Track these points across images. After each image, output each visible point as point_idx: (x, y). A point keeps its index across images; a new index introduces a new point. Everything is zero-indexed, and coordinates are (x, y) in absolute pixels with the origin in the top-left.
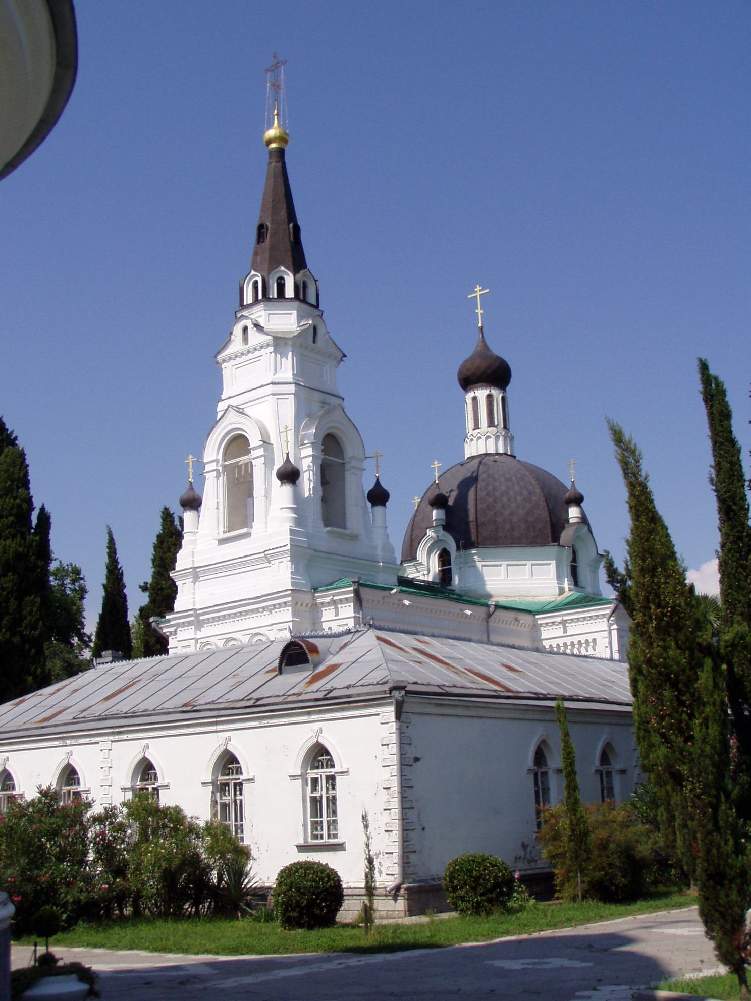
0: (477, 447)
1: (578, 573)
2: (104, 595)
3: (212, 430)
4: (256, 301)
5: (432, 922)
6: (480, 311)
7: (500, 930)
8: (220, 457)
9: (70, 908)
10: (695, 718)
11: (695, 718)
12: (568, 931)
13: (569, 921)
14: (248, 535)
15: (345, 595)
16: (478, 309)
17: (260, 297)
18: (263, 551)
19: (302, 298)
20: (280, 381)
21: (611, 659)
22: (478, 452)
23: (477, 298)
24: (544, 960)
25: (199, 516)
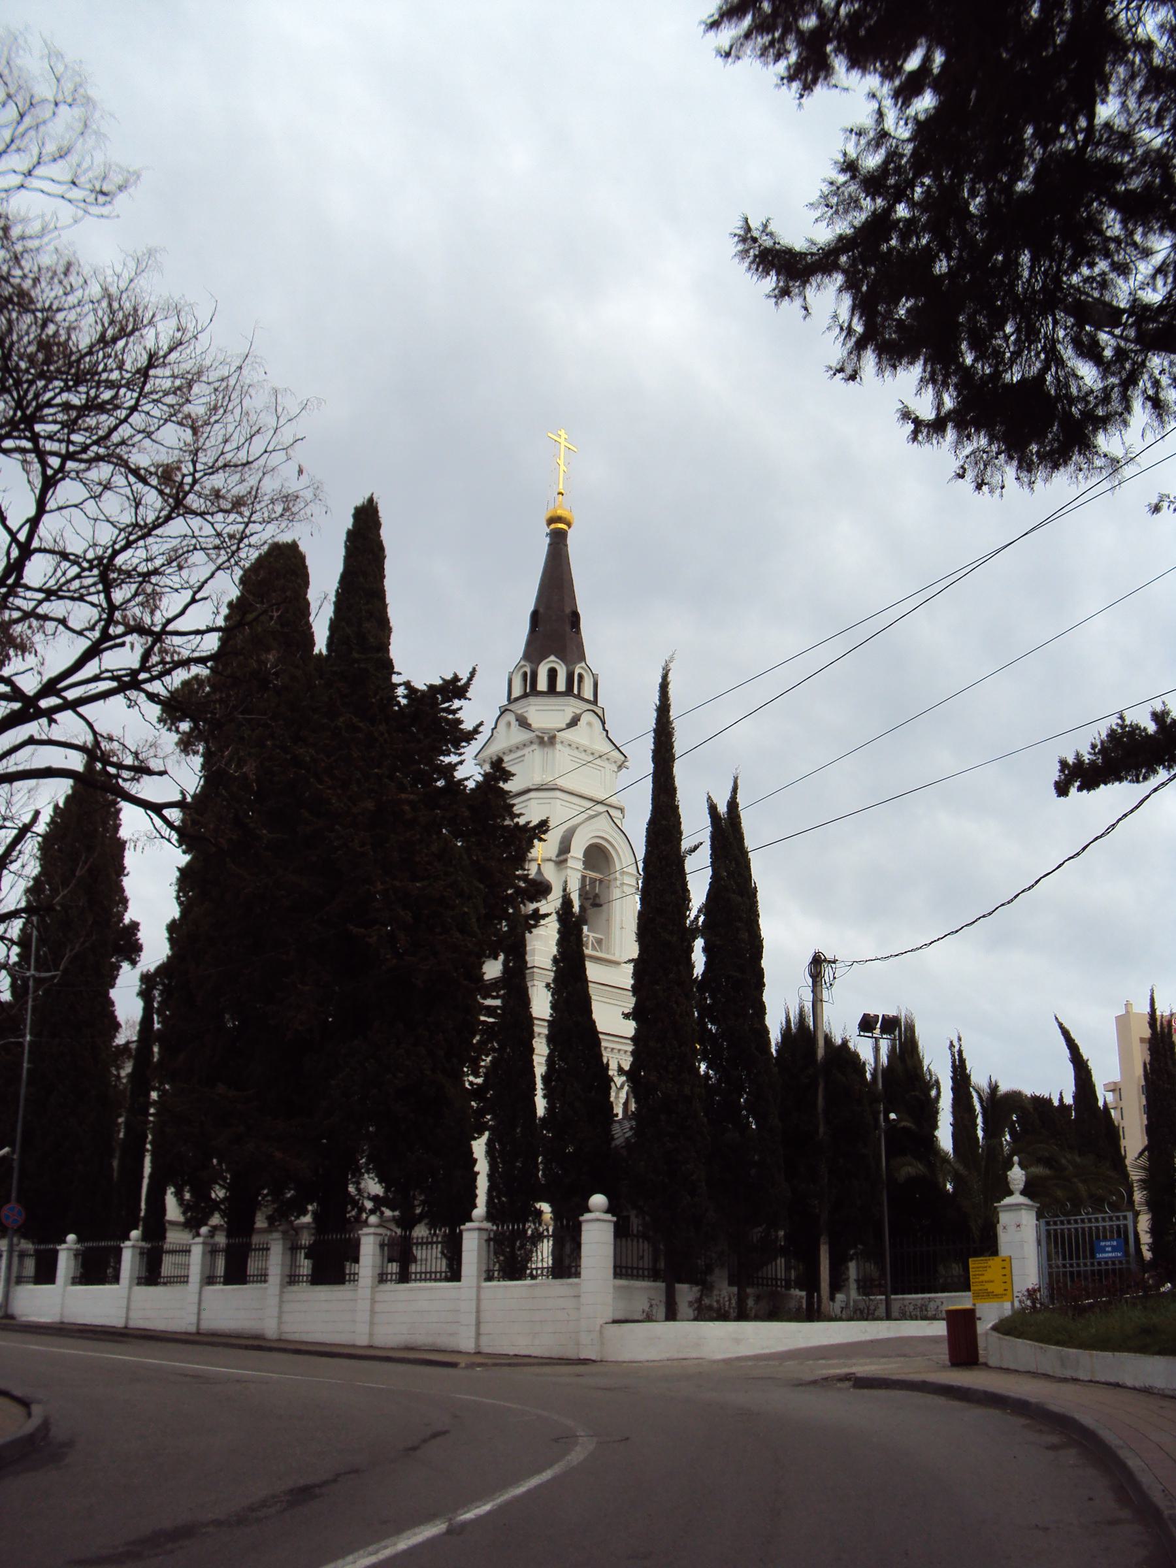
4: (569, 691)
17: (528, 691)
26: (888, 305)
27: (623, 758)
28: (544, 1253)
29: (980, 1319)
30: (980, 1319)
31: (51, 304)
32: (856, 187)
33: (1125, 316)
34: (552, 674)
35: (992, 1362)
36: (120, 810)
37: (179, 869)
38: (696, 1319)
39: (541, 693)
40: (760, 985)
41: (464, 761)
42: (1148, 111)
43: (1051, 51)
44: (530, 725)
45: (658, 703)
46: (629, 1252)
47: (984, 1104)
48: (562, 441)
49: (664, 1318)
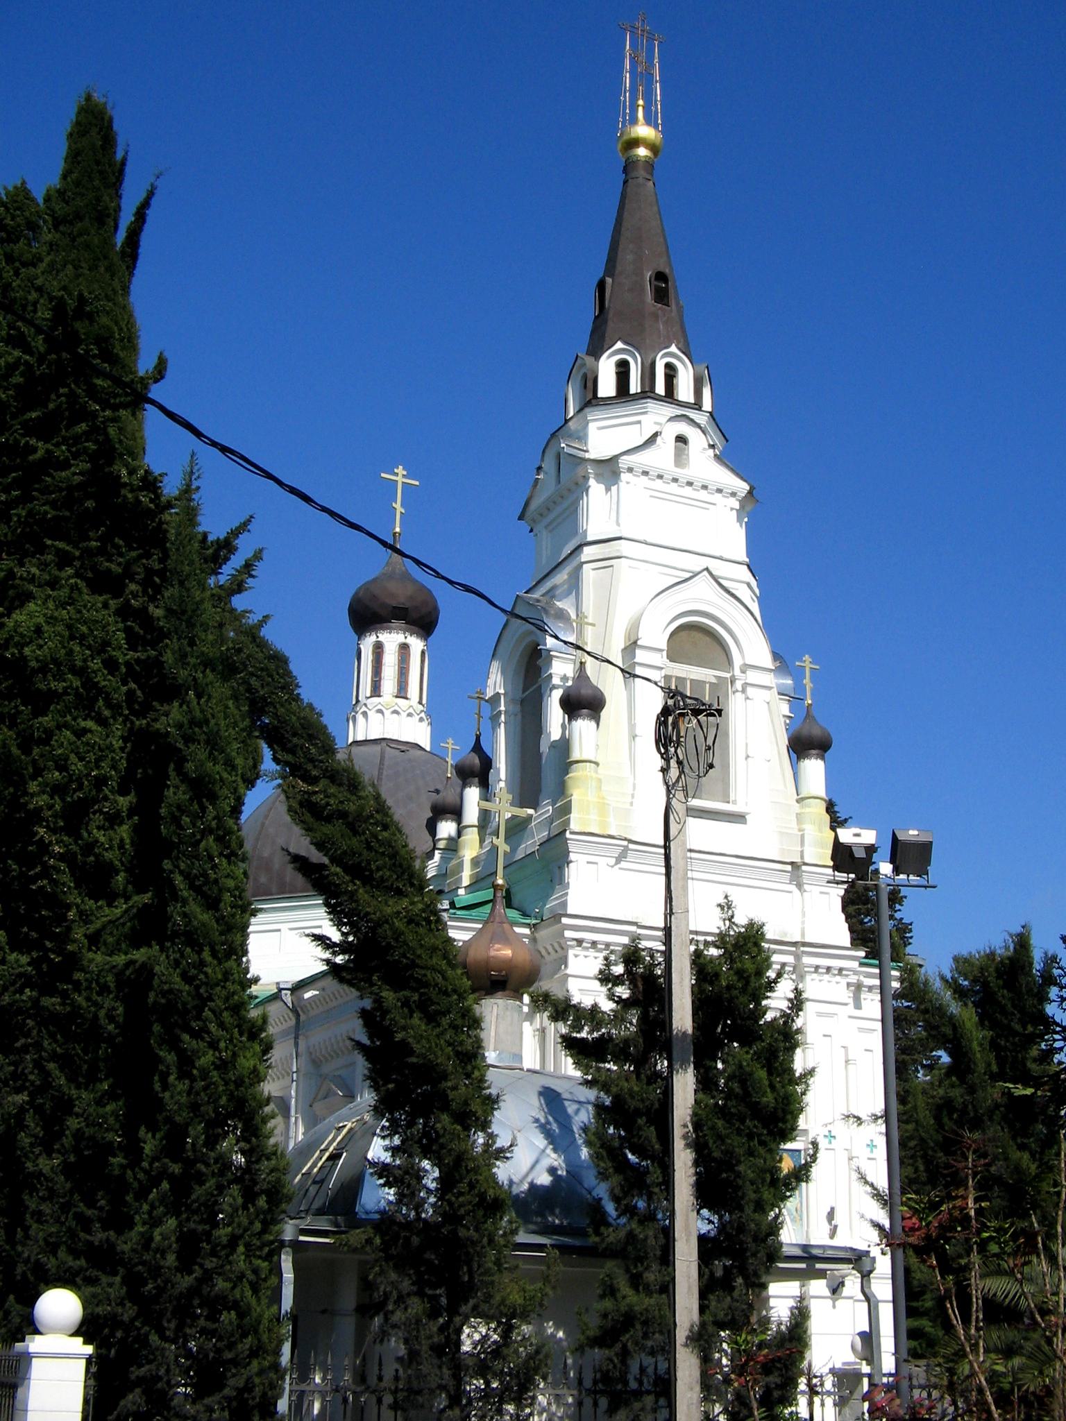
4: (648, 392)
12: (684, 1090)
29: (249, 531)
30: (249, 531)
33: (99, 382)
34: (623, 370)
35: (515, 906)
39: (607, 401)
42: (413, 1308)
43: (424, 1088)
48: (400, 479)
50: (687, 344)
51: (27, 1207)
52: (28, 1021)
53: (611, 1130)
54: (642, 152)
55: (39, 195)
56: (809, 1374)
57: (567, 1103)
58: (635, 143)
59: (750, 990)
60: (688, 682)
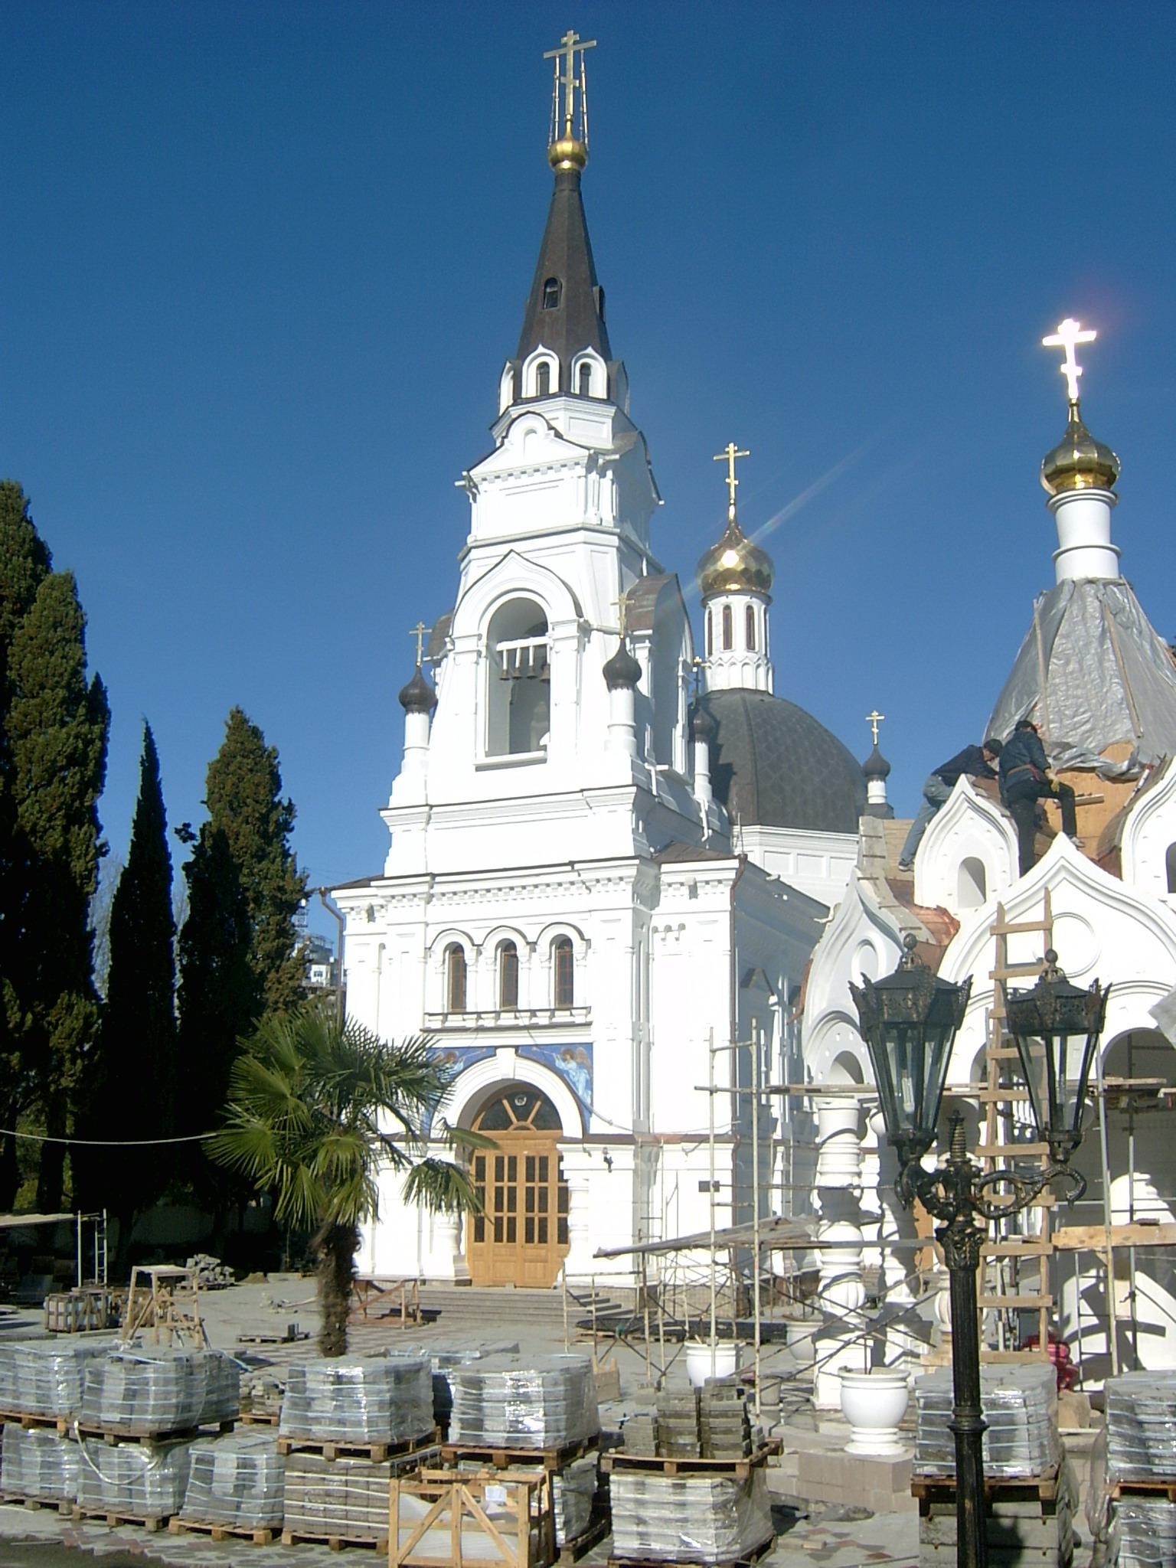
0: (627, 1533)
1: (1060, 534)
2: (355, 1255)
3: (836, 1188)
4: (544, 394)
5: (735, 504)
6: (732, 481)
7: (497, 1477)
8: (484, 631)
9: (364, 1402)
10: (939, 1156)
11: (939, 1156)
12: (490, 1198)
13: (325, 1432)
14: (543, 761)
15: (533, 1229)
16: (729, 477)
17: (554, 387)
18: (593, 1272)
19: (577, 391)
20: (561, 529)
21: (943, 1089)
22: (949, 1381)
23: (1111, 1361)
24: (480, 1119)
25: (431, 722)
26: (949, 1144)
27: (512, 554)
28: (201, 1376)
31: (35, 824)
32: (385, 1387)
34: (544, 368)
36: (437, 1425)
37: (735, 774)
38: (1092, 860)
40: (142, 787)
41: (840, 1369)
44: (147, 747)
45: (127, 866)
46: (460, 1309)
47: (787, 1510)
49: (508, 750)
50: (1026, 1079)
51: (12, 1054)
52: (40, 1137)
53: (566, 147)
54: (566, 165)
55: (250, 724)
56: (748, 1487)
57: (1091, 1313)
58: (557, 161)
59: (95, 1310)
60: (734, 1334)
